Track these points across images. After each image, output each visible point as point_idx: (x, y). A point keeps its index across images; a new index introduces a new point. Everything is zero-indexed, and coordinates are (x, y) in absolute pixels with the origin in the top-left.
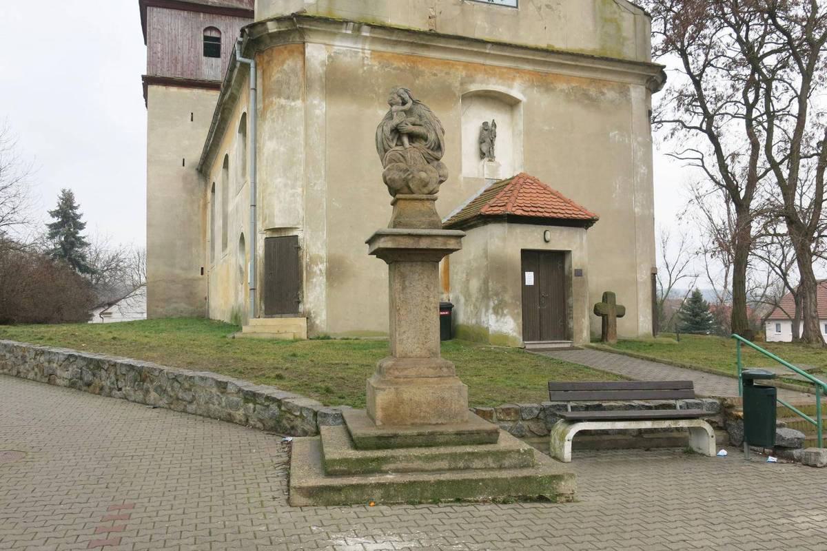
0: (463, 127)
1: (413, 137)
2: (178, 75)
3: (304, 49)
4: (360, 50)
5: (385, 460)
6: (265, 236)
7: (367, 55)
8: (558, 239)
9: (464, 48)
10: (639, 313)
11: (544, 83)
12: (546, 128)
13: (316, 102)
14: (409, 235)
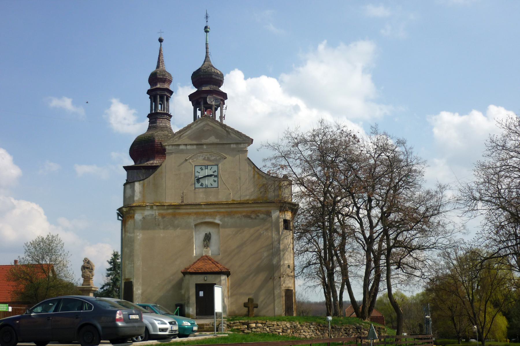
1: (87, 268)
6: (124, 281)
11: (230, 214)
13: (138, 234)
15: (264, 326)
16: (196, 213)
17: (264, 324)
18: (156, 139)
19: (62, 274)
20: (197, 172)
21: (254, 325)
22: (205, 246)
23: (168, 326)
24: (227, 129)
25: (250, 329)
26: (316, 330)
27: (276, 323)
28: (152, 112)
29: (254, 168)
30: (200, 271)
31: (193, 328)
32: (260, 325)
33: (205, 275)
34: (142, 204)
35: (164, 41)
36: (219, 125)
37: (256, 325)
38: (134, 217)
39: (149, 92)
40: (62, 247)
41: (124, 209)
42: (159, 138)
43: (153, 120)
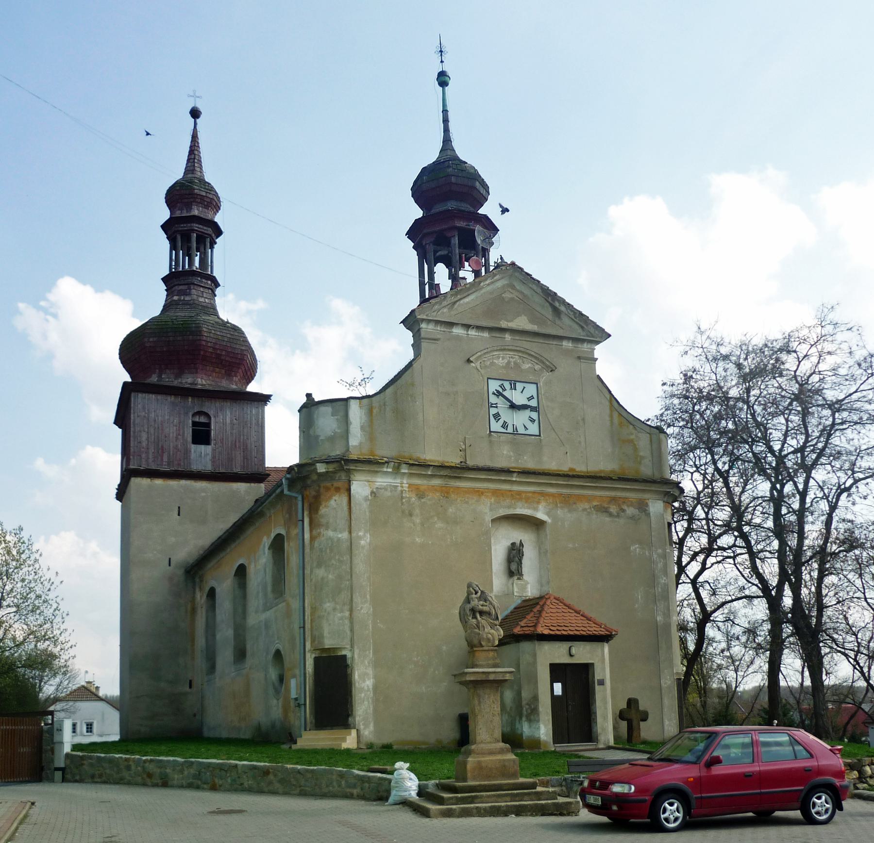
0: (493, 548)
2: (165, 468)
3: (350, 486)
4: (399, 485)
5: (476, 797)
6: (313, 656)
7: (405, 489)
8: (582, 653)
9: (493, 478)
11: (567, 501)
12: (571, 546)
13: (361, 534)
14: (483, 673)
18: (205, 329)
24: (557, 304)
35: (202, 116)
36: (539, 291)
39: (165, 227)
42: (210, 328)
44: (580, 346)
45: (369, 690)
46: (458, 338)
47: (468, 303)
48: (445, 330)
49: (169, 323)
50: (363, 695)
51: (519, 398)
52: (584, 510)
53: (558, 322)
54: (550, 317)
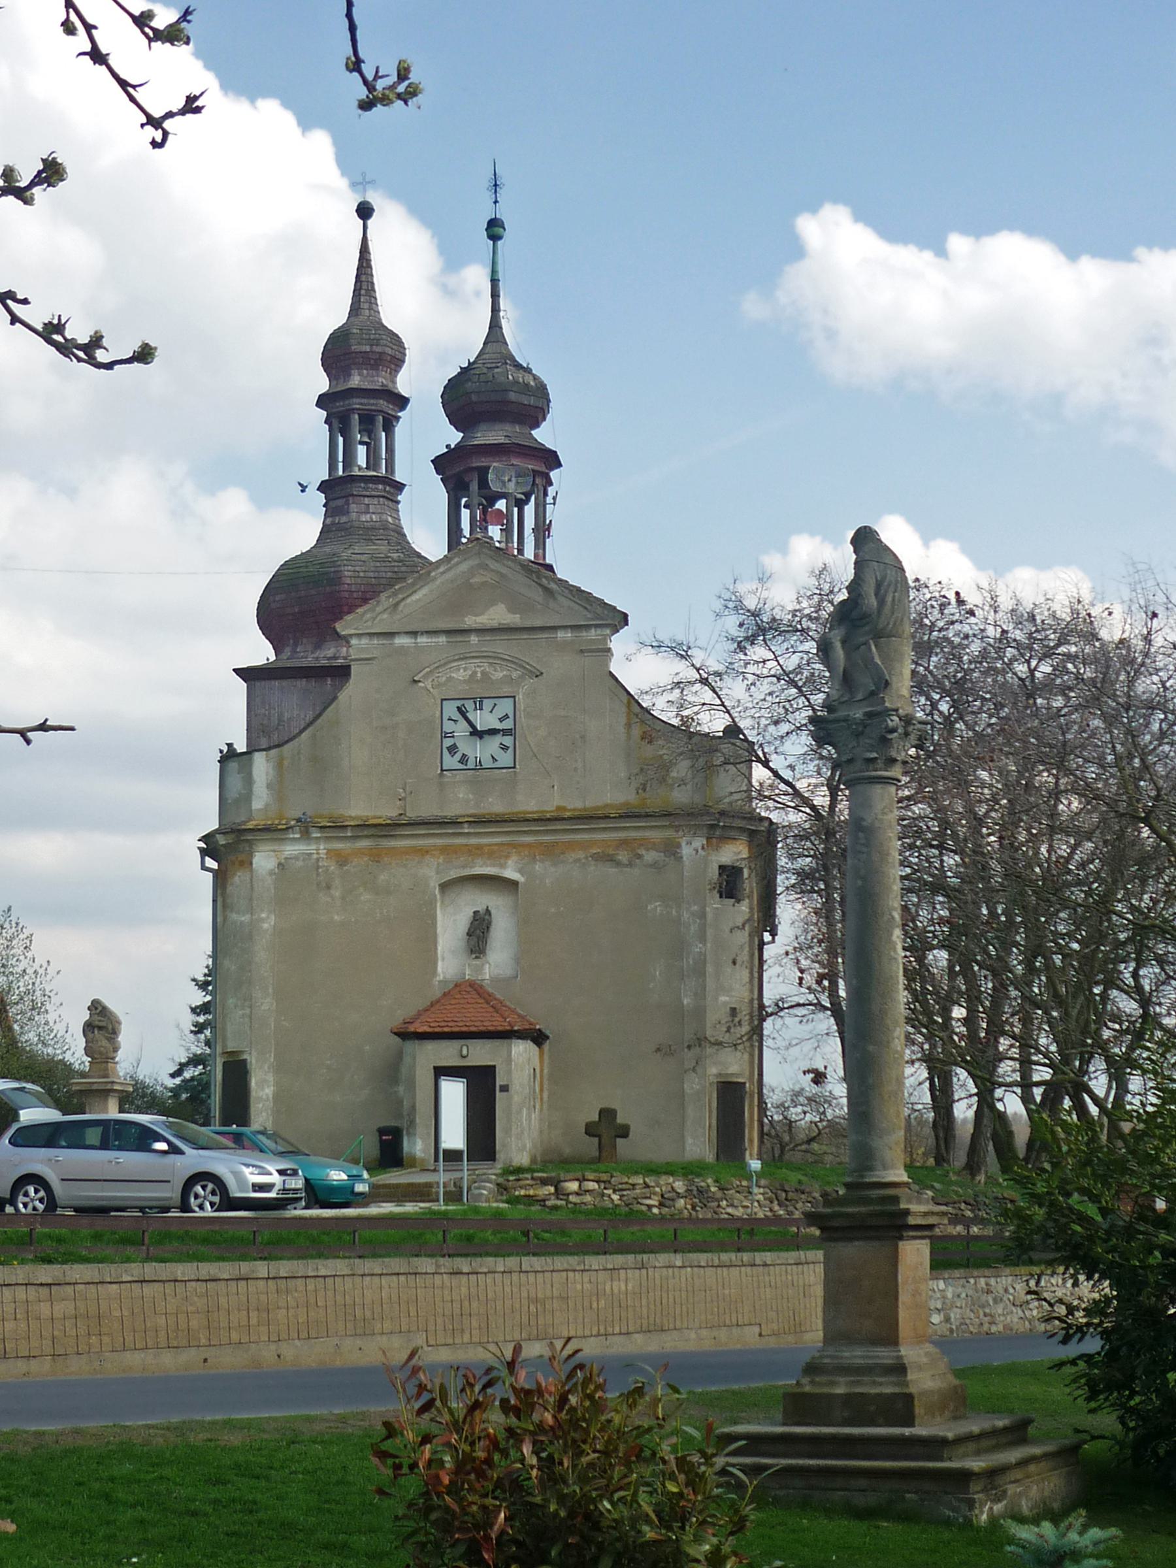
1: (100, 1028)
10: (686, 1134)
11: (550, 852)
12: (553, 910)
13: (263, 915)
15: (605, 1188)
16: (444, 850)
17: (604, 1182)
19: (32, 1036)
20: (450, 719)
21: (574, 1186)
22: (472, 952)
23: (275, 1178)
25: (561, 1197)
26: (772, 1202)
27: (641, 1181)
28: (335, 475)
29: (629, 705)
30: (446, 1029)
31: (353, 1187)
32: (592, 1185)
33: (463, 1042)
34: (277, 822)
36: (518, 568)
37: (580, 1185)
38: (251, 864)
40: (26, 948)
41: (221, 840)
42: (357, 569)
43: (340, 502)
44: (585, 634)
45: (268, 1099)
46: (402, 650)
47: (419, 600)
48: (385, 642)
49: (301, 570)
50: (261, 1105)
51: (483, 719)
52: (578, 860)
53: (552, 604)
54: (540, 599)
